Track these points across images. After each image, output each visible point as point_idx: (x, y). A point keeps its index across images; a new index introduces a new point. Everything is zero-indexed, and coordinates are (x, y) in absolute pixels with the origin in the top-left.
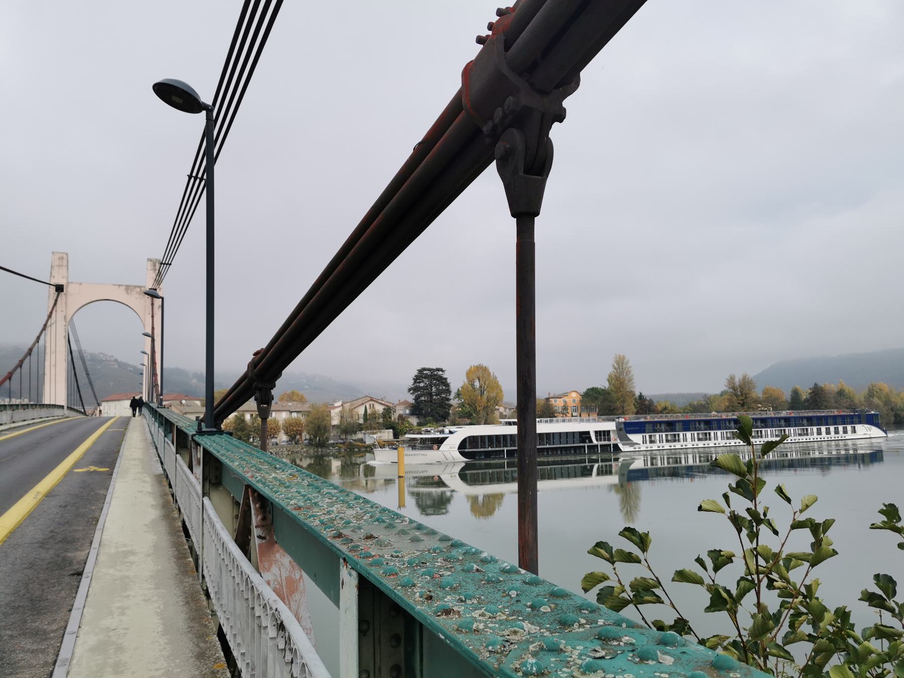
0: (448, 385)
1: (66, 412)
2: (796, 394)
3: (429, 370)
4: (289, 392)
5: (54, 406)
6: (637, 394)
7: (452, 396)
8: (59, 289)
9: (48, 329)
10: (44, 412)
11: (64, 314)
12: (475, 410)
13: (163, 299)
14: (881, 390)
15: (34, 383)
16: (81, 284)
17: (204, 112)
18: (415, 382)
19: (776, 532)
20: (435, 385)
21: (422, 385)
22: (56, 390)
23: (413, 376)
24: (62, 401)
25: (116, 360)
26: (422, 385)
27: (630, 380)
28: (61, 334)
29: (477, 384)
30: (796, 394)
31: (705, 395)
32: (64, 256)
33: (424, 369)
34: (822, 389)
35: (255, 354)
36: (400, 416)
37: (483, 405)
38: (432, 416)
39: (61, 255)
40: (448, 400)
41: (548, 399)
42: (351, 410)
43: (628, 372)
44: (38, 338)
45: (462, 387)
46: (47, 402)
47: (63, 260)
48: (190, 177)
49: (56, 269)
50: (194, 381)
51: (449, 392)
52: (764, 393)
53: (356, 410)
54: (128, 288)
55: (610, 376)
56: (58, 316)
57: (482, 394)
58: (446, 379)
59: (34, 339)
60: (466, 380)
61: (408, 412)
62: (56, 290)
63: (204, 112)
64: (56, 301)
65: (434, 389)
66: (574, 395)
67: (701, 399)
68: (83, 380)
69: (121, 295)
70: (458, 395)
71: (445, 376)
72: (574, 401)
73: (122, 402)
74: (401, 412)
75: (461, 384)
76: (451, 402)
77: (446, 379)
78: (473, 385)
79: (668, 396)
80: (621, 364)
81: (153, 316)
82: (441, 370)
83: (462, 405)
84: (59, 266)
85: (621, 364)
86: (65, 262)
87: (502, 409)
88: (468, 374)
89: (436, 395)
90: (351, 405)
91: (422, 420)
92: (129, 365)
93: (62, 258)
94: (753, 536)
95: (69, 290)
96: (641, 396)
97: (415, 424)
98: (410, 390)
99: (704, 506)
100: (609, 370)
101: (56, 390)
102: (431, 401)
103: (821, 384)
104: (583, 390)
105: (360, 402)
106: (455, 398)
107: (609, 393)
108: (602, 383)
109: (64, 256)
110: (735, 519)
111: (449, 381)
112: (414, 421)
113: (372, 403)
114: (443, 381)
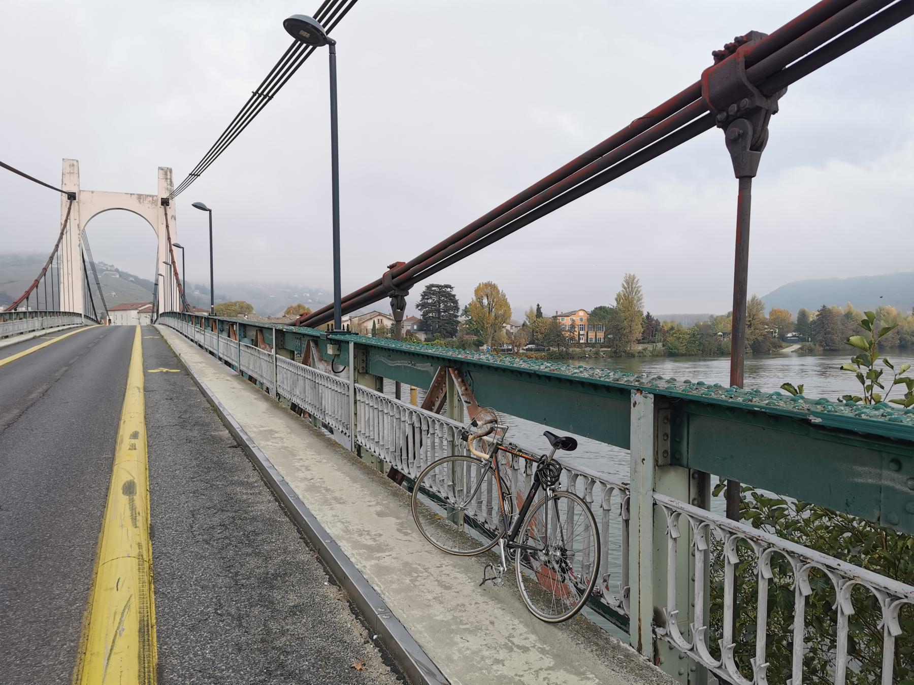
0: (456, 302)
1: (84, 320)
2: (803, 315)
3: (438, 286)
4: (295, 305)
5: (74, 314)
6: (645, 314)
7: (459, 314)
8: (72, 197)
9: (64, 236)
10: (58, 320)
11: (77, 222)
12: (483, 327)
13: (210, 211)
14: (888, 313)
15: (56, 289)
16: (92, 192)
17: (327, 46)
18: (423, 298)
19: (882, 387)
20: (443, 302)
21: (430, 301)
22: (73, 299)
23: (421, 292)
24: (79, 309)
25: (117, 270)
26: (430, 301)
27: (639, 300)
28: (75, 241)
29: (485, 301)
30: (803, 315)
31: (712, 316)
32: (75, 163)
33: (433, 286)
34: (830, 312)
35: (391, 267)
36: (408, 331)
37: (490, 322)
38: (440, 332)
39: (72, 162)
40: (456, 316)
41: (555, 317)
42: (359, 325)
43: (638, 292)
44: (57, 246)
45: (470, 305)
46: (62, 310)
47: (72, 167)
48: (271, 98)
49: (67, 175)
50: (197, 293)
51: (457, 308)
52: (771, 314)
53: (365, 324)
54: (140, 196)
55: (619, 295)
56: (72, 224)
57: (490, 311)
58: (454, 296)
59: (53, 247)
60: (474, 298)
61: (415, 327)
62: (69, 199)
63: (327, 46)
64: (70, 209)
65: (442, 306)
66: (581, 313)
67: (707, 319)
68: (93, 287)
69: (133, 204)
70: (466, 311)
71: (453, 293)
72: (581, 320)
73: (128, 312)
74: (409, 328)
75: (470, 301)
76: (459, 319)
77: (454, 296)
78: (481, 303)
79: (673, 317)
80: (630, 283)
81: (167, 226)
82: (451, 288)
83: (469, 322)
84: (70, 173)
85: (630, 283)
86: (76, 171)
87: (508, 327)
88: (477, 291)
89: (445, 312)
90: (359, 320)
91: (430, 336)
92: (131, 276)
93: (73, 165)
94: (869, 388)
95: (81, 197)
96: (648, 316)
97: (423, 339)
98: (418, 306)
99: (845, 367)
100: (618, 288)
101: (73, 299)
102: (439, 318)
103: (829, 306)
104: (590, 309)
105: (368, 317)
106: (462, 315)
107: (617, 313)
108: (610, 302)
109: (75, 163)
110: (860, 377)
111: (457, 298)
112: (422, 336)
113: (380, 318)
114: (452, 298)
